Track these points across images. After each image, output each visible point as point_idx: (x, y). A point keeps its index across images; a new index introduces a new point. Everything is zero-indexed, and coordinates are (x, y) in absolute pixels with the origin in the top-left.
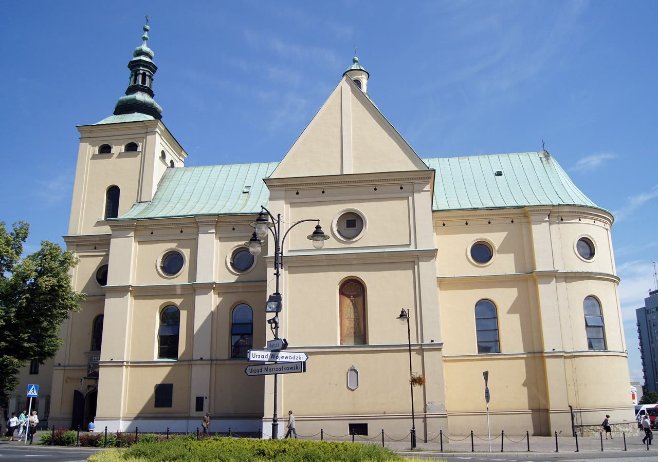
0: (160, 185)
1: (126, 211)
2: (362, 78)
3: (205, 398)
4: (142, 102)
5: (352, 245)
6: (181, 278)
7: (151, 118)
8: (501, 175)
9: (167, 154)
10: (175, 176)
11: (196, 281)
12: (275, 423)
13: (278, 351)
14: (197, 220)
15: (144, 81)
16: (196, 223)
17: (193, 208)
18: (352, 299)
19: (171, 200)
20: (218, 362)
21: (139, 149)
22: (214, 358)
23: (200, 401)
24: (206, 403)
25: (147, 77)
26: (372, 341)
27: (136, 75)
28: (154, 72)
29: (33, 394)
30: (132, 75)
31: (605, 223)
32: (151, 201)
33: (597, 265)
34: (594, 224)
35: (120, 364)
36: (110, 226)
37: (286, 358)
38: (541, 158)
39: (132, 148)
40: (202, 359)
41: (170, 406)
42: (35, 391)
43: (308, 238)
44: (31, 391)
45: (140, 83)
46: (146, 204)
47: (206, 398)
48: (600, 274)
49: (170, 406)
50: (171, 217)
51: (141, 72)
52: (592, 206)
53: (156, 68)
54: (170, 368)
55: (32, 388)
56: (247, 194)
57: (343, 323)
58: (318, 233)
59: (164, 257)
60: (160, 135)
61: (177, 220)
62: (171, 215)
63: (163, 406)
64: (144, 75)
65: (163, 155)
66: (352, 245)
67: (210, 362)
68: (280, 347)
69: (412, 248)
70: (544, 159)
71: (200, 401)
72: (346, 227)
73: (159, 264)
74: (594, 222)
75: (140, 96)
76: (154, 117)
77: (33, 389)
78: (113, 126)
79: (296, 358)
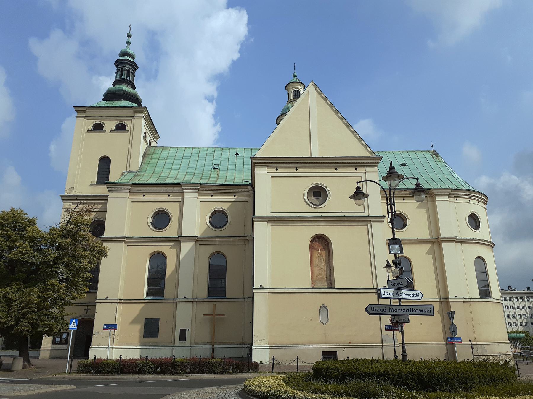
0: (143, 159)
1: (114, 177)
2: (301, 88)
3: (187, 330)
4: (128, 92)
5: (319, 210)
6: (170, 231)
7: (136, 105)
8: (406, 166)
9: (147, 135)
10: (154, 153)
11: (181, 235)
12: (404, 354)
13: (400, 289)
14: (183, 187)
15: (128, 75)
16: (182, 189)
17: (176, 178)
18: (320, 251)
19: (155, 171)
20: (198, 300)
21: (128, 129)
22: (195, 297)
23: (183, 333)
24: (188, 334)
25: (131, 74)
26: (338, 284)
27: (122, 71)
28: (136, 70)
29: (73, 327)
30: (118, 71)
31: (478, 201)
32: (138, 171)
33: (483, 233)
34: (478, 204)
35: (116, 301)
36: (108, 188)
37: (407, 295)
38: (432, 155)
39: (121, 128)
40: (185, 297)
41: (157, 336)
42: (75, 325)
43: (350, 197)
44: (72, 325)
45: (125, 78)
46: (135, 173)
47: (188, 330)
48: (473, 239)
49: (157, 336)
50: (161, 183)
51: (127, 69)
52: (470, 189)
53: (137, 67)
54: (143, 304)
55: (73, 322)
56: (217, 170)
57: (313, 270)
58: (359, 194)
59: (154, 213)
60: (144, 119)
61: (165, 186)
62: (151, 182)
63: (151, 337)
64: (128, 71)
65: (145, 137)
66: (319, 210)
67: (192, 300)
68: (405, 284)
69: (366, 214)
70: (434, 156)
71: (183, 333)
72: (313, 197)
73: (150, 220)
74: (469, 201)
75: (126, 88)
76: (138, 105)
77: (74, 322)
78: (110, 109)
79: (414, 295)
